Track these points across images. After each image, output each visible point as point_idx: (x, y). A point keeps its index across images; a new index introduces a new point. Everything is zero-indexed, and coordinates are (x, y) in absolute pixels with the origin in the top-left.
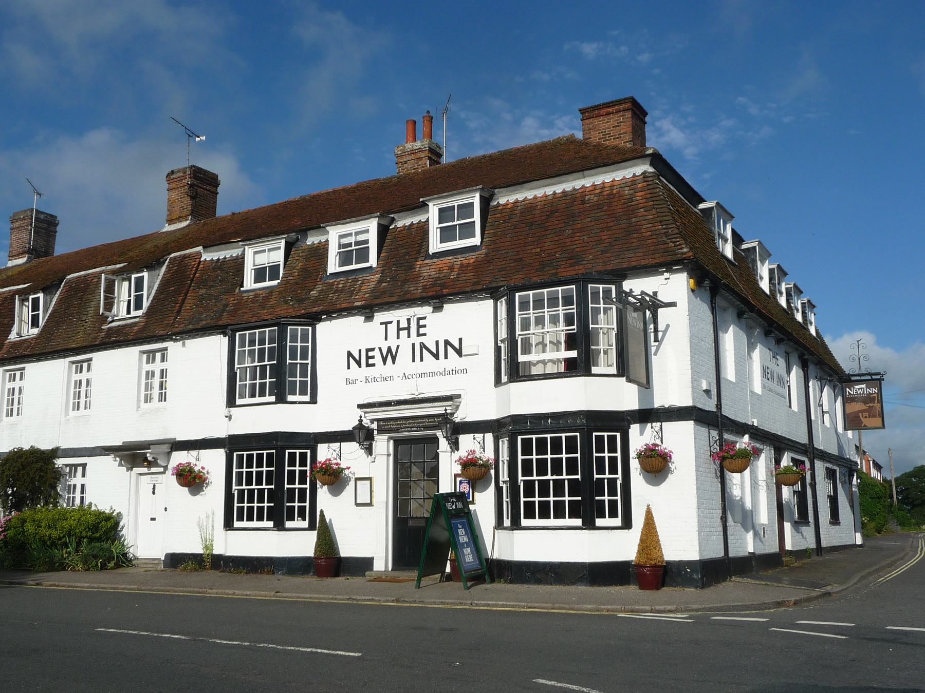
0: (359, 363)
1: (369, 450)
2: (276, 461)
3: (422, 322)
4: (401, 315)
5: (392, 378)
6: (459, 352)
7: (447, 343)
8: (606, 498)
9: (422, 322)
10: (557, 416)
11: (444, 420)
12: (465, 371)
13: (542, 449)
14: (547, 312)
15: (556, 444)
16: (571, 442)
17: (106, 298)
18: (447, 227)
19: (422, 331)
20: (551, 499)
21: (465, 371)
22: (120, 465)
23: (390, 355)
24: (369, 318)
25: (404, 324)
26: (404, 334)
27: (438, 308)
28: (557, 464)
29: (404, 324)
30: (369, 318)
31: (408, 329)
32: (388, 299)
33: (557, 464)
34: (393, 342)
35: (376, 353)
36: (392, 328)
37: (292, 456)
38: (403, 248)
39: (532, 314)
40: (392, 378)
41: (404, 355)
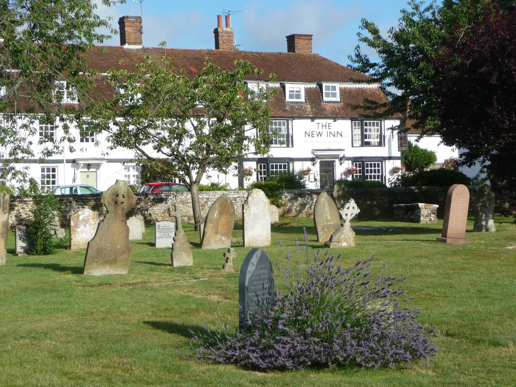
0: (309, 136)
2: (362, 165)
6: (341, 135)
7: (338, 132)
10: (375, 157)
11: (336, 157)
14: (372, 128)
15: (281, 166)
16: (285, 166)
18: (333, 92)
23: (320, 134)
24: (312, 121)
25: (324, 125)
26: (324, 128)
27: (335, 121)
29: (324, 125)
30: (312, 121)
32: (320, 116)
34: (320, 130)
35: (315, 133)
36: (320, 125)
37: (272, 166)
38: (315, 97)
39: (368, 127)
41: (324, 134)
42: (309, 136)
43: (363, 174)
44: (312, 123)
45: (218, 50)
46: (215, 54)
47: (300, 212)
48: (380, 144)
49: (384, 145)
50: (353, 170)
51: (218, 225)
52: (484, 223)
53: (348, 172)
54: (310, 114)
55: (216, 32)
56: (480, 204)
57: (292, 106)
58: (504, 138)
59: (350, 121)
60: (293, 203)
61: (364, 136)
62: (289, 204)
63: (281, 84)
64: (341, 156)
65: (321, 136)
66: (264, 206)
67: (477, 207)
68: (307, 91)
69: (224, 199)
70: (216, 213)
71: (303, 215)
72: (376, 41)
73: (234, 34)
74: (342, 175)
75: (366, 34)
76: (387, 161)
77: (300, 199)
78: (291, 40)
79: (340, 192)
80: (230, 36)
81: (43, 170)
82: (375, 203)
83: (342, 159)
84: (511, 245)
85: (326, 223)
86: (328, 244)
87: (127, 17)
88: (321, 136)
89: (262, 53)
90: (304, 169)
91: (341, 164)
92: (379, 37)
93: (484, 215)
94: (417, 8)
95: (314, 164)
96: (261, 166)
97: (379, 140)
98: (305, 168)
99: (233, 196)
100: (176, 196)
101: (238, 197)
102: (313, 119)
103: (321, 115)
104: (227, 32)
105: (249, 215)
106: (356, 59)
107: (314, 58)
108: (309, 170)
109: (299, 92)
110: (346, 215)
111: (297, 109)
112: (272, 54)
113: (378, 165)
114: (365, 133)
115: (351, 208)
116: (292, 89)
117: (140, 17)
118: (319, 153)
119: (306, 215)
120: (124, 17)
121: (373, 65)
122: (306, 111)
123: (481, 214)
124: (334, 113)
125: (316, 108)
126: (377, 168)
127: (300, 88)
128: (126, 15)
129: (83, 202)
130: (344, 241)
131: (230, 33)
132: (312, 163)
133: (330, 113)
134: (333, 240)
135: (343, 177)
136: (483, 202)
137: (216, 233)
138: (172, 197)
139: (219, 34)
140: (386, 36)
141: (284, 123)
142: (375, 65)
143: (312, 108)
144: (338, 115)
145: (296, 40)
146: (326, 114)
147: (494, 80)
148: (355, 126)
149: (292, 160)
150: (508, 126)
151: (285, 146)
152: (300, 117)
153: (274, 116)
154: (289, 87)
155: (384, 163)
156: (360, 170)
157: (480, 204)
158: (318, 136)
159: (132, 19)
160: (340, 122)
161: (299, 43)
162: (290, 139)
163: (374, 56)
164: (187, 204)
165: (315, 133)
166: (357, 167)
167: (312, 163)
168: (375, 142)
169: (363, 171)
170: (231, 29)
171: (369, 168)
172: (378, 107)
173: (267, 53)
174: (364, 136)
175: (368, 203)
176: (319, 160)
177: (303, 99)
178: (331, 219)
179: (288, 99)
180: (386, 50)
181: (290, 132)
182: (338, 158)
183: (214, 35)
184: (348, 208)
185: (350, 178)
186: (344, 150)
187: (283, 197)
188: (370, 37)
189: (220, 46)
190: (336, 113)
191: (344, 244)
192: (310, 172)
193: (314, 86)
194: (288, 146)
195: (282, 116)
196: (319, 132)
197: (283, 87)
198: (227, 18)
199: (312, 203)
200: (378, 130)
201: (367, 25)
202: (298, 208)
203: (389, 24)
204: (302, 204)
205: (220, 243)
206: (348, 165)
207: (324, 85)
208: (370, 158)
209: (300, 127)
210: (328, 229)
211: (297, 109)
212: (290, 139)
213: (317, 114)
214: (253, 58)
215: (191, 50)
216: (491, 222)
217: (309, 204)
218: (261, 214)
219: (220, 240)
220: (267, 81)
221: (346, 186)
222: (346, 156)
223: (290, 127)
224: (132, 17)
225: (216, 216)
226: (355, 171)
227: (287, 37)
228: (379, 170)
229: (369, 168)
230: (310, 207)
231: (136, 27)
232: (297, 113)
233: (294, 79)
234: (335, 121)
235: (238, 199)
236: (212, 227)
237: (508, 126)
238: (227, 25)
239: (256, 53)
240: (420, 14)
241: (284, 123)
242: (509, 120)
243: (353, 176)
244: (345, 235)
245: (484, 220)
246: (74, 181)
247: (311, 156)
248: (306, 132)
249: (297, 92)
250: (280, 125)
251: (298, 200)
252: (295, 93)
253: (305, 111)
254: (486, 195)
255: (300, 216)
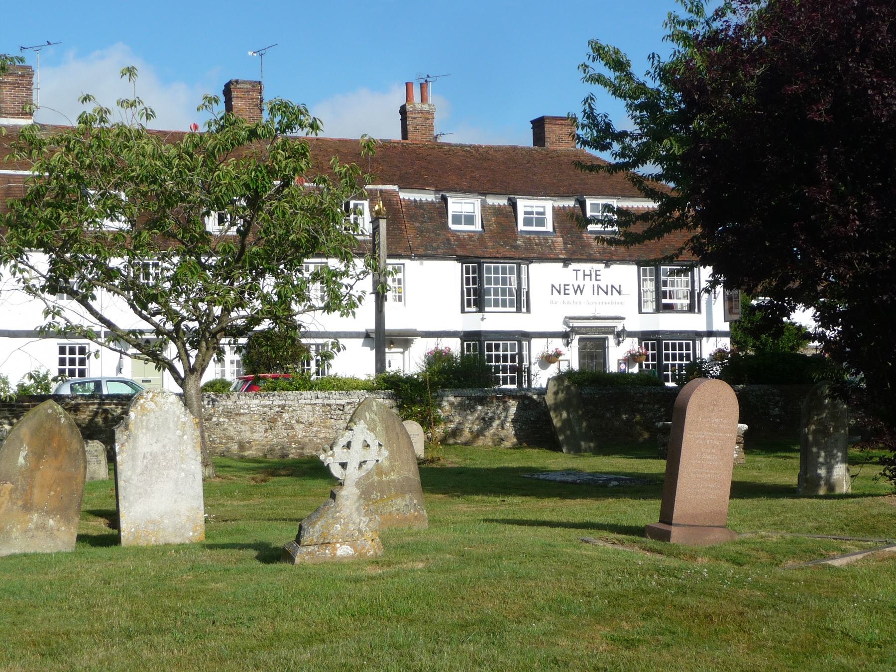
0: (559, 292)
1: (46, 317)
2: (658, 346)
3: (598, 273)
4: (587, 267)
5: (580, 303)
6: (619, 293)
7: (612, 286)
8: (492, 297)
9: (598, 273)
10: (681, 332)
11: (610, 330)
12: (622, 303)
13: (674, 349)
17: (594, 333)
19: (598, 278)
20: (500, 276)
21: (622, 303)
22: (364, 345)
23: (579, 290)
24: (566, 265)
25: (587, 272)
26: (587, 278)
27: (607, 266)
28: (674, 356)
29: (587, 272)
30: (566, 265)
31: (590, 275)
32: (579, 257)
33: (674, 356)
34: (580, 282)
35: (570, 287)
36: (580, 274)
38: (573, 222)
40: (580, 303)
41: (588, 290)
42: (559, 292)
43: (660, 361)
44: (565, 269)
45: (407, 141)
46: (395, 147)
47: (480, 433)
48: (691, 309)
49: (699, 311)
50: (640, 355)
51: (32, 487)
52: (822, 472)
53: (632, 359)
54: (562, 254)
55: (403, 111)
56: (813, 427)
57: (529, 239)
58: (849, 264)
59: (636, 267)
60: (465, 417)
61: (660, 294)
62: (457, 419)
63: (509, 199)
64: (620, 328)
65: (581, 292)
66: (179, 433)
67: (806, 435)
68: (557, 212)
69: (48, 415)
70: (23, 454)
71: (486, 441)
72: (627, 88)
73: (435, 115)
74: (620, 364)
75: (600, 68)
76: (705, 339)
77: (480, 408)
78: (539, 125)
79: (561, 396)
80: (428, 119)
81: (62, 350)
82: (638, 417)
83: (620, 335)
84: (844, 553)
85: (376, 478)
86: (290, 549)
87: (237, 82)
88: (581, 292)
89: (480, 146)
90: (550, 352)
91: (619, 343)
92: (629, 77)
93: (823, 454)
94: (699, 11)
95: (568, 344)
96: (469, 346)
97: (688, 302)
98: (551, 351)
99: (338, 402)
100: (214, 401)
101: (348, 404)
102: (566, 262)
103: (581, 254)
104: (422, 112)
105: (133, 458)
106: (586, 122)
107: (576, 156)
108: (558, 354)
109: (543, 213)
110: (344, 465)
111: (536, 245)
112: (498, 149)
113: (688, 345)
114: (663, 289)
115: (357, 445)
116: (529, 209)
117: (260, 83)
118: (577, 324)
119: (494, 441)
120: (230, 82)
121: (621, 136)
122: (555, 248)
123: (815, 450)
124: (605, 253)
125: (573, 243)
126: (684, 352)
127: (544, 207)
128: (234, 78)
129: (11, 411)
130: (344, 542)
131: (428, 112)
132: (565, 341)
133: (599, 252)
134: (306, 539)
135: (623, 367)
136: (820, 422)
137: (27, 507)
138: (206, 402)
139: (408, 115)
140: (642, 71)
141: (511, 269)
142: (624, 134)
143: (565, 243)
144: (612, 255)
145: (547, 127)
146: (591, 254)
147: (820, 113)
148: (645, 275)
149: (527, 336)
150: (857, 231)
151: (514, 309)
152: (542, 259)
153: (492, 255)
154: (524, 205)
155: (698, 342)
156: (653, 355)
157: (813, 427)
158: (576, 293)
159: (246, 86)
160: (616, 268)
161: (553, 132)
162: (524, 298)
163: (621, 117)
164: (238, 418)
165: (570, 287)
166: (647, 350)
167: (565, 341)
168: (682, 305)
169: (658, 357)
170: (429, 105)
171: (670, 352)
172: (631, 221)
173: (490, 148)
174: (661, 295)
175: (624, 417)
176: (578, 337)
177: (549, 227)
178: (392, 468)
179: (521, 227)
180: (646, 104)
181: (524, 286)
182: (612, 333)
183: (400, 117)
184: (348, 445)
185: (635, 370)
186: (624, 319)
187: (445, 404)
188: (610, 74)
189: (410, 136)
190: (610, 253)
191: (344, 551)
192: (560, 358)
193: (570, 203)
194: (519, 310)
195: (509, 256)
196: (579, 287)
197: (514, 205)
198: (423, 87)
199: (506, 417)
200: (687, 282)
201: (599, 51)
202: (476, 427)
203: (649, 49)
204: (483, 419)
205: (41, 534)
206: (631, 345)
207: (589, 202)
208: (672, 332)
209: (542, 276)
210: (382, 492)
211: (536, 245)
212: (524, 298)
213: (574, 253)
214: (464, 156)
215: (351, 141)
216: (840, 471)
217: (499, 418)
218: (170, 455)
219: (42, 527)
220: (484, 194)
221: (574, 383)
222: (628, 329)
223: (524, 276)
224: (244, 82)
225: (21, 460)
226: (644, 357)
227: (532, 122)
228: (688, 356)
229: (670, 352)
230: (502, 426)
231: (252, 99)
232: (538, 251)
233: (533, 192)
234: (607, 266)
235: (347, 408)
236: (12, 491)
237: (857, 231)
238: (423, 99)
239: (470, 146)
240: (707, 22)
241: (511, 269)
242: (861, 216)
243: (641, 366)
244: (346, 524)
245: (822, 464)
246: (120, 370)
247: (562, 328)
248: (553, 286)
249: (538, 213)
250: (504, 272)
251: (475, 410)
252: (535, 216)
253: (551, 248)
254: (826, 407)
255: (480, 442)
